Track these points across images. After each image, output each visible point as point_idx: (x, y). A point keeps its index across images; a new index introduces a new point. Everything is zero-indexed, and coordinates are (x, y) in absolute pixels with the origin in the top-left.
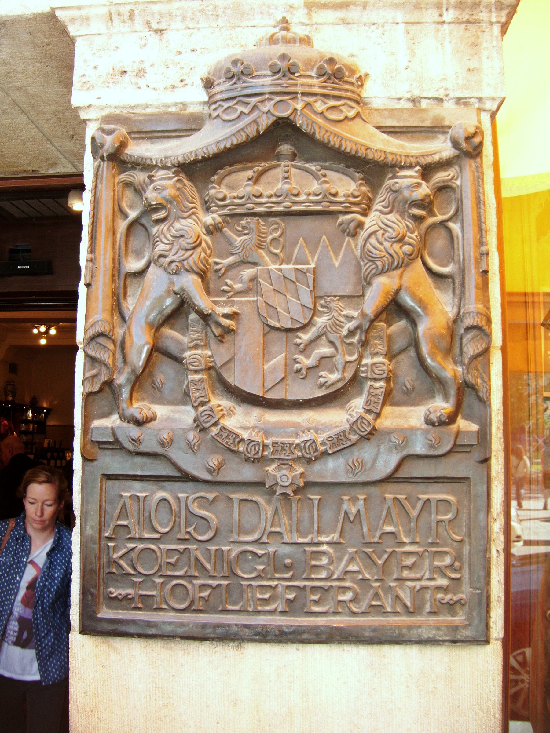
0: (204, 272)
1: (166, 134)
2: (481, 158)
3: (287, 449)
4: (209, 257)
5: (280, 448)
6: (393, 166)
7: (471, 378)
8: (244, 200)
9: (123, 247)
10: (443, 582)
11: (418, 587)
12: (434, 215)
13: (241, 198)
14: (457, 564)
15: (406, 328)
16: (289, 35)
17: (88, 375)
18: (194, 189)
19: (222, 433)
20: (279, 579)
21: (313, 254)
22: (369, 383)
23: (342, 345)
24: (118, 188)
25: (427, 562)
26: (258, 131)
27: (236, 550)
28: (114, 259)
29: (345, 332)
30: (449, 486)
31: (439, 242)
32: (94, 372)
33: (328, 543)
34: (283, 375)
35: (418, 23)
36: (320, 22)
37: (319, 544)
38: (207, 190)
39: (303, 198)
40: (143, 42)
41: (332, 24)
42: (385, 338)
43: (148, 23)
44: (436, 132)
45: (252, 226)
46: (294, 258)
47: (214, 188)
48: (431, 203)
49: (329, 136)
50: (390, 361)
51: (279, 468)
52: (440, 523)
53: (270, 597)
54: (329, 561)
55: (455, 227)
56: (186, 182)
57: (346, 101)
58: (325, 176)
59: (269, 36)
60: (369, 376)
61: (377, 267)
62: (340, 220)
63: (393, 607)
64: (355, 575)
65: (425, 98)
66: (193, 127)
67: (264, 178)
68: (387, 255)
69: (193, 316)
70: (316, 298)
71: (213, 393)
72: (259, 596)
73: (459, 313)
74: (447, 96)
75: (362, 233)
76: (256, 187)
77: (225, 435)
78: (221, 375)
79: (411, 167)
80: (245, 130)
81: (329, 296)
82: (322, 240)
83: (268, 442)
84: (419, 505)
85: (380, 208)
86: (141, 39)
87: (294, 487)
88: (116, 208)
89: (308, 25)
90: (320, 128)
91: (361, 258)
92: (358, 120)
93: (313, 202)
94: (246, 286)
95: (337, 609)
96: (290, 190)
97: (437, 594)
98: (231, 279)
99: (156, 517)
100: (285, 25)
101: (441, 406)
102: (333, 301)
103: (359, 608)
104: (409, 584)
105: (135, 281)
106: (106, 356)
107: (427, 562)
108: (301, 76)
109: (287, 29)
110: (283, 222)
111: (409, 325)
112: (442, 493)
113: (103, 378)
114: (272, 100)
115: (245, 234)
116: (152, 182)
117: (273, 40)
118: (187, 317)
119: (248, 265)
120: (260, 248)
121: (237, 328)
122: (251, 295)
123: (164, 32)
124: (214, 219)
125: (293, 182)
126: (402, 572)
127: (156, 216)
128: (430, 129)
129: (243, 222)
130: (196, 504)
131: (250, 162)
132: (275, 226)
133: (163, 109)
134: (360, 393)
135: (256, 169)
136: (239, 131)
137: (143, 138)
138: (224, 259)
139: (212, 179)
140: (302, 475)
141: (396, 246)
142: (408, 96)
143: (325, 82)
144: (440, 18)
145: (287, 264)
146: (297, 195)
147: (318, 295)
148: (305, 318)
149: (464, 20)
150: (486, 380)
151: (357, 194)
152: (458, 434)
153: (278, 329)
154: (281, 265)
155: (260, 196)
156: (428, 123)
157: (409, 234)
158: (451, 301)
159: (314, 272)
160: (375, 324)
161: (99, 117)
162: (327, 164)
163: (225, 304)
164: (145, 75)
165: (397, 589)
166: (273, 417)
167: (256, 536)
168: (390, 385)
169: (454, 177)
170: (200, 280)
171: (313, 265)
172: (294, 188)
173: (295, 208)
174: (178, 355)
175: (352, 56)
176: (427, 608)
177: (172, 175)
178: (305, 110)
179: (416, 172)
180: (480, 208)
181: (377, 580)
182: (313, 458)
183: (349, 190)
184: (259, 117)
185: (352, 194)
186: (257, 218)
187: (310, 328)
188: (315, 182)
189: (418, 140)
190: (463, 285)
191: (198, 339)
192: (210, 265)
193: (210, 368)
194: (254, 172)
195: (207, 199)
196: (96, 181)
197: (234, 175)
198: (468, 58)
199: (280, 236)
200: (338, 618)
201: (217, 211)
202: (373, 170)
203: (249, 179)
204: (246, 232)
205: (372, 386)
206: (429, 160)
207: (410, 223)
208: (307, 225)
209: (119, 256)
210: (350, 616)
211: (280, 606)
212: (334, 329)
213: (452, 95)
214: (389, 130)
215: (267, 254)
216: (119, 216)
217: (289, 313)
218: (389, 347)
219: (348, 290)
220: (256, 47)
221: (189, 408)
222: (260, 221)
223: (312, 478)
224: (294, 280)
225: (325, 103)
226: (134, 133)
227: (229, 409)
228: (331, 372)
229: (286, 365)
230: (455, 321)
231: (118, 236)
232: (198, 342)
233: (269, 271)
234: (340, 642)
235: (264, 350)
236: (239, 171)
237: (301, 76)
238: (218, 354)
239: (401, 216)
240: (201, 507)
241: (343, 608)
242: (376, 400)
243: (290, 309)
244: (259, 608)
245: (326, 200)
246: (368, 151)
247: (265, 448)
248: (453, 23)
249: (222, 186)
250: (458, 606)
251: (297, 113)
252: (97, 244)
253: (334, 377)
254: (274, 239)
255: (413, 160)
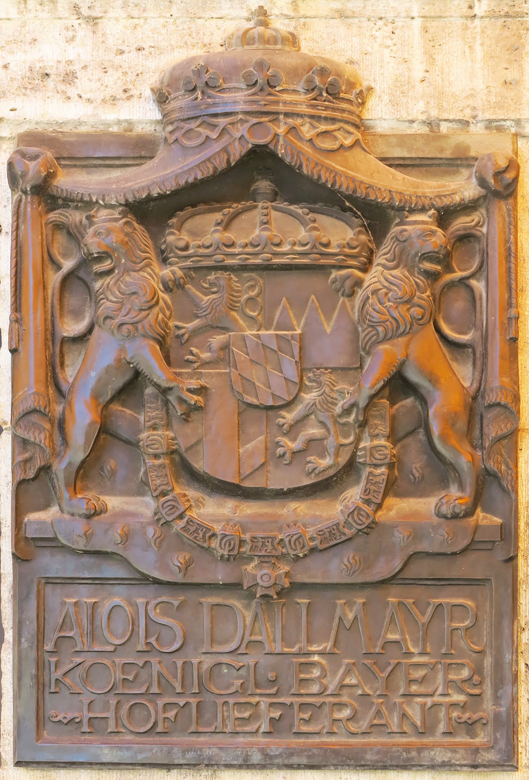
0: (163, 338)
1: (108, 162)
2: (516, 198)
3: (269, 544)
4: (169, 319)
5: (260, 544)
6: (401, 209)
7: (492, 464)
8: (211, 249)
9: (57, 307)
10: (459, 698)
11: (429, 704)
12: (452, 271)
13: (208, 247)
14: (476, 678)
15: (414, 407)
16: (268, 33)
17: (20, 458)
18: (146, 234)
19: (190, 527)
20: (261, 695)
21: (298, 318)
22: (368, 469)
23: (335, 425)
24: (48, 231)
25: (440, 677)
26: (228, 161)
27: (208, 662)
28: (46, 320)
29: (338, 410)
30: (467, 589)
31: (458, 304)
32: (27, 455)
33: (320, 653)
34: (263, 460)
35: (440, 17)
36: (309, 14)
37: (310, 654)
38: (164, 236)
39: (286, 248)
40: (70, 34)
41: (326, 17)
42: (388, 418)
43: (76, 7)
44: (458, 166)
45: (222, 282)
46: (275, 322)
47: (173, 234)
48: (448, 255)
49: (320, 170)
50: (395, 444)
51: (259, 567)
52: (456, 632)
53: (250, 716)
54: (321, 674)
55: (478, 285)
56: (136, 225)
57: (342, 124)
58: (314, 221)
59: (241, 33)
60: (368, 462)
61: (378, 334)
62: (333, 276)
63: (400, 726)
64: (354, 689)
65: (445, 120)
66: (143, 153)
67: (236, 224)
68: (391, 319)
69: (149, 390)
70: (302, 372)
71: (177, 482)
72: (237, 715)
73: (479, 388)
74: (474, 117)
75: (360, 293)
76: (226, 234)
77: (192, 529)
78: (187, 460)
79: (423, 210)
80: (212, 160)
81: (318, 369)
82: (310, 301)
83: (247, 537)
84: (430, 611)
85: (384, 261)
86: (67, 29)
87: (278, 588)
88: (46, 256)
89: (293, 18)
90: (308, 159)
91: (359, 322)
92: (357, 151)
93: (298, 254)
94: (215, 355)
95: (332, 728)
96: (270, 238)
97: (452, 712)
98: (196, 347)
99: (108, 626)
100: (262, 18)
101: (456, 496)
102: (324, 373)
103: (359, 728)
104: (419, 699)
105: (74, 347)
106: (42, 436)
107: (440, 677)
108: (282, 91)
109: (265, 24)
110: (262, 278)
111: (417, 403)
112: (458, 597)
113: (38, 463)
114: (247, 121)
115: (214, 293)
116: (91, 224)
117: (246, 39)
118: (142, 393)
119: (218, 330)
120: (232, 309)
121: (205, 405)
122: (222, 366)
123: (98, 21)
124: (174, 273)
125: (274, 228)
126: (409, 686)
127: (98, 268)
128: (450, 162)
129: (212, 277)
130: (158, 611)
131: (218, 202)
132: (251, 283)
133: (102, 127)
134: (357, 481)
135: (226, 211)
136: (204, 162)
137: (75, 166)
138: (188, 323)
139: (170, 222)
140: (287, 574)
141: (403, 309)
142: (424, 117)
143: (315, 99)
144: (469, 11)
145: (267, 330)
146: (278, 245)
147: (305, 366)
148: (289, 394)
149: (502, 13)
150: (512, 466)
151: (355, 243)
152: (477, 528)
153: (256, 407)
154: (258, 330)
155: (233, 245)
156: (448, 154)
157: (418, 293)
158: (470, 375)
159: (301, 339)
160: (375, 400)
161: (14, 135)
162: (317, 206)
163: (190, 376)
164: (75, 80)
165: (404, 706)
166: (250, 509)
167: (233, 646)
168: (394, 473)
169: (479, 222)
170: (158, 347)
171: (299, 331)
172: (275, 235)
173: (276, 261)
174: (132, 439)
175: (352, 62)
176: (442, 727)
177: (117, 216)
178: (289, 136)
179: (430, 217)
180: (510, 262)
181: (380, 696)
182: (301, 555)
183: (344, 239)
184: (230, 144)
185: (348, 244)
186: (228, 273)
187: (296, 406)
188: (302, 228)
189: (435, 175)
190: (485, 355)
191: (157, 418)
192: (170, 329)
193: (173, 452)
194: (223, 215)
195: (163, 247)
196: (17, 220)
197: (198, 217)
198: (505, 66)
199: (258, 295)
200: (333, 739)
201: (177, 263)
202: (375, 216)
203: (219, 224)
204: (215, 289)
205: (370, 473)
206: (447, 201)
207: (421, 280)
208: (292, 282)
209: (52, 316)
210: (348, 737)
211: (263, 726)
212: (325, 407)
213: (480, 117)
214: (397, 162)
215: (242, 318)
216: (50, 267)
217: (270, 388)
218: (393, 430)
219: (342, 361)
220: (224, 48)
221: (148, 499)
222: (232, 276)
223: (301, 578)
224: (276, 348)
225: (315, 128)
226: (64, 158)
227: (198, 500)
228: (322, 456)
229: (266, 449)
230: (474, 398)
231: (50, 292)
232: (157, 421)
233: (244, 338)
234: (336, 767)
235: (239, 431)
236: (204, 212)
237: (282, 91)
238: (183, 436)
239: (409, 271)
240: (164, 613)
241: (339, 728)
242: (376, 489)
243: (270, 382)
244: (238, 729)
245: (315, 251)
246: (370, 190)
247: (242, 544)
248: (487, 17)
249: (182, 231)
250: (478, 725)
251: (278, 141)
252: (23, 301)
253: (327, 462)
254: (250, 299)
255: (427, 202)
